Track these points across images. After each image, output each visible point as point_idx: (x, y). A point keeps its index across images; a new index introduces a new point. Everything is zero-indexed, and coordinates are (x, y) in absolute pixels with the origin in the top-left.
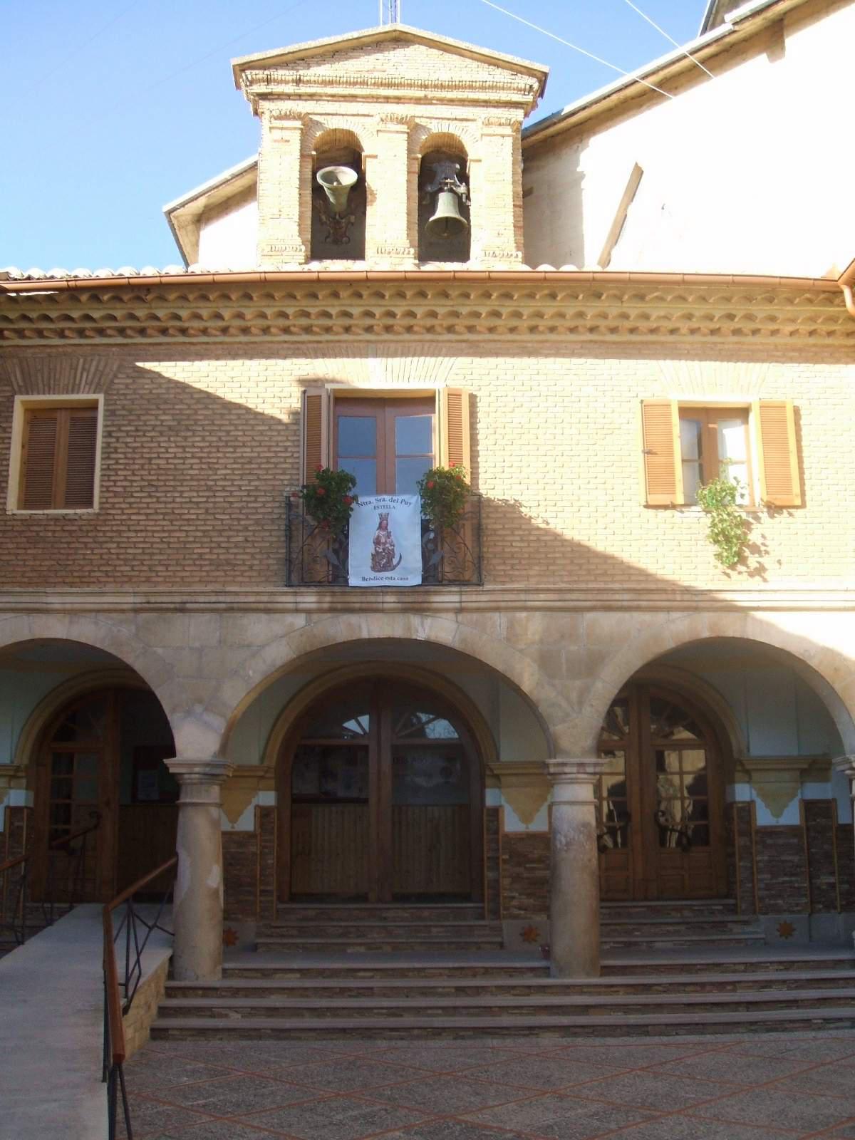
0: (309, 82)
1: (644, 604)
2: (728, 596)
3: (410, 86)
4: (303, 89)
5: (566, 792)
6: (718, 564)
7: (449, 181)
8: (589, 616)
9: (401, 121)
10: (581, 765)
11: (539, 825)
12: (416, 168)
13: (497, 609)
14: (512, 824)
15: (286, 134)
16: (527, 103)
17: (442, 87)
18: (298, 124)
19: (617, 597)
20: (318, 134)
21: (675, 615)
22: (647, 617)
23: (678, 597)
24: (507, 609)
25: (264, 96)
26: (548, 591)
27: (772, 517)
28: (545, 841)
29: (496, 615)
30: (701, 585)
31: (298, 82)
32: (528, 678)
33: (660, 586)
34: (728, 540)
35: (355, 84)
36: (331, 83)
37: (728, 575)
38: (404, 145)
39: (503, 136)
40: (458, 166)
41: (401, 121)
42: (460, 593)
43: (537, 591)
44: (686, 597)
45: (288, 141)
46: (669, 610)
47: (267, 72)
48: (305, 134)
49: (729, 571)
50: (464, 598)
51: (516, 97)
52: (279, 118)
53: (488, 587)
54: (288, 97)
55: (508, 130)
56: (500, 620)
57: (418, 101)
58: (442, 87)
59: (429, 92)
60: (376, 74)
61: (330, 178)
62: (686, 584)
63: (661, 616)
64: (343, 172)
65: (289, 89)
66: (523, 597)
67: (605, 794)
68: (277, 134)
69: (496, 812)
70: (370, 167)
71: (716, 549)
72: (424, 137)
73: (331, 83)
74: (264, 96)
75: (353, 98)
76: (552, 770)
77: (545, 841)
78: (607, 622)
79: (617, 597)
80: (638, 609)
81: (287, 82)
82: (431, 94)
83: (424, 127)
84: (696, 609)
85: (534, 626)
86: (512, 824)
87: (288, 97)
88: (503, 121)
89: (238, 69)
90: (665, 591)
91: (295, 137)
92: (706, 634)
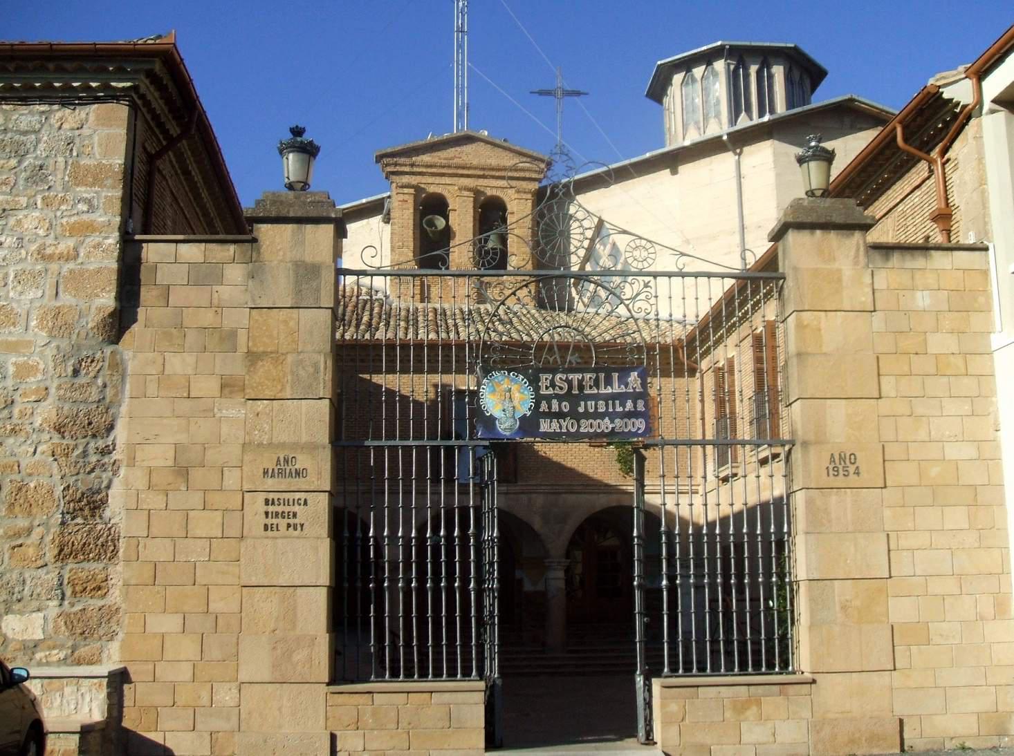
0: (419, 165)
1: (795, 98)
2: (624, 488)
3: (475, 168)
4: (416, 169)
5: (552, 574)
6: (621, 472)
7: (496, 223)
8: (564, 495)
9: (469, 190)
10: (559, 562)
11: (540, 587)
12: (478, 217)
13: (522, 493)
14: (528, 587)
15: (406, 197)
16: (540, 179)
17: (493, 169)
18: (412, 191)
19: (575, 488)
20: (423, 195)
21: (601, 495)
22: (586, 496)
23: (603, 488)
24: (527, 493)
25: (393, 173)
26: (547, 485)
27: (646, 451)
28: (544, 594)
29: (523, 496)
30: (613, 483)
31: (412, 165)
32: (537, 524)
33: (591, 483)
34: (625, 462)
35: (444, 167)
36: (431, 166)
37: (625, 477)
38: (471, 205)
39: (527, 200)
40: (501, 213)
41: (469, 190)
42: (507, 486)
43: (541, 485)
44: (607, 488)
45: (407, 201)
46: (598, 493)
47: (395, 159)
48: (416, 197)
49: (626, 476)
50: (509, 488)
51: (534, 176)
52: (402, 187)
53: (519, 483)
54: (406, 173)
55: (529, 196)
56: (524, 497)
57: (479, 177)
58: (493, 169)
59: (487, 172)
60: (455, 161)
61: (431, 224)
62: (606, 482)
63: (595, 497)
64: (438, 219)
65: (407, 169)
66: (535, 488)
67: (788, 574)
68: (401, 197)
69: (520, 581)
70: (452, 216)
71: (619, 465)
72: (482, 198)
73: (431, 166)
74: (393, 173)
75: (443, 175)
76: (547, 564)
77: (544, 594)
78: (571, 498)
79: (575, 488)
80: (585, 493)
81: (406, 165)
82: (487, 173)
83: (483, 192)
84: (610, 493)
85: (539, 500)
86: (528, 587)
87: (406, 173)
88: (527, 190)
89: (378, 158)
90: (596, 485)
91: (411, 200)
92: (614, 504)
